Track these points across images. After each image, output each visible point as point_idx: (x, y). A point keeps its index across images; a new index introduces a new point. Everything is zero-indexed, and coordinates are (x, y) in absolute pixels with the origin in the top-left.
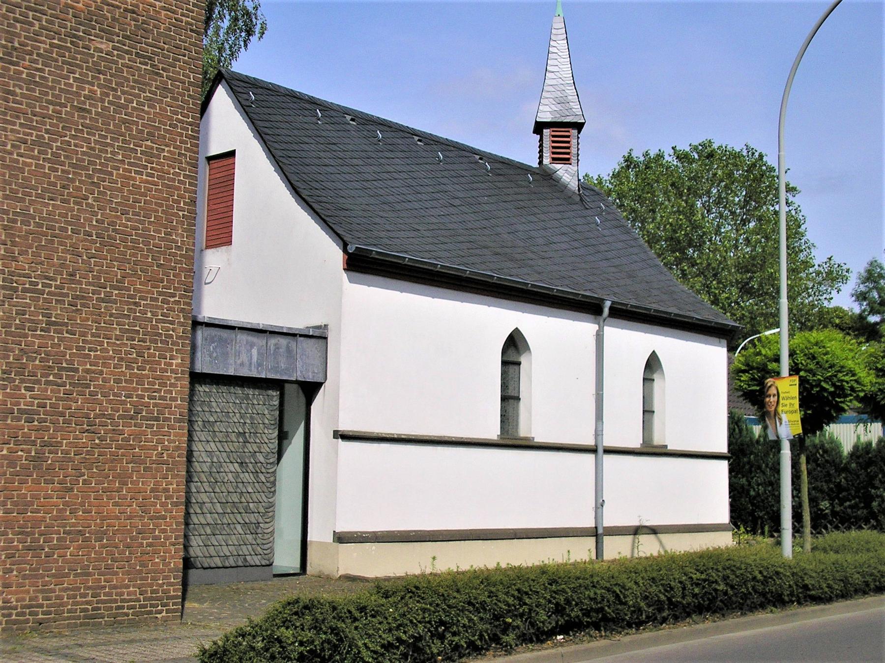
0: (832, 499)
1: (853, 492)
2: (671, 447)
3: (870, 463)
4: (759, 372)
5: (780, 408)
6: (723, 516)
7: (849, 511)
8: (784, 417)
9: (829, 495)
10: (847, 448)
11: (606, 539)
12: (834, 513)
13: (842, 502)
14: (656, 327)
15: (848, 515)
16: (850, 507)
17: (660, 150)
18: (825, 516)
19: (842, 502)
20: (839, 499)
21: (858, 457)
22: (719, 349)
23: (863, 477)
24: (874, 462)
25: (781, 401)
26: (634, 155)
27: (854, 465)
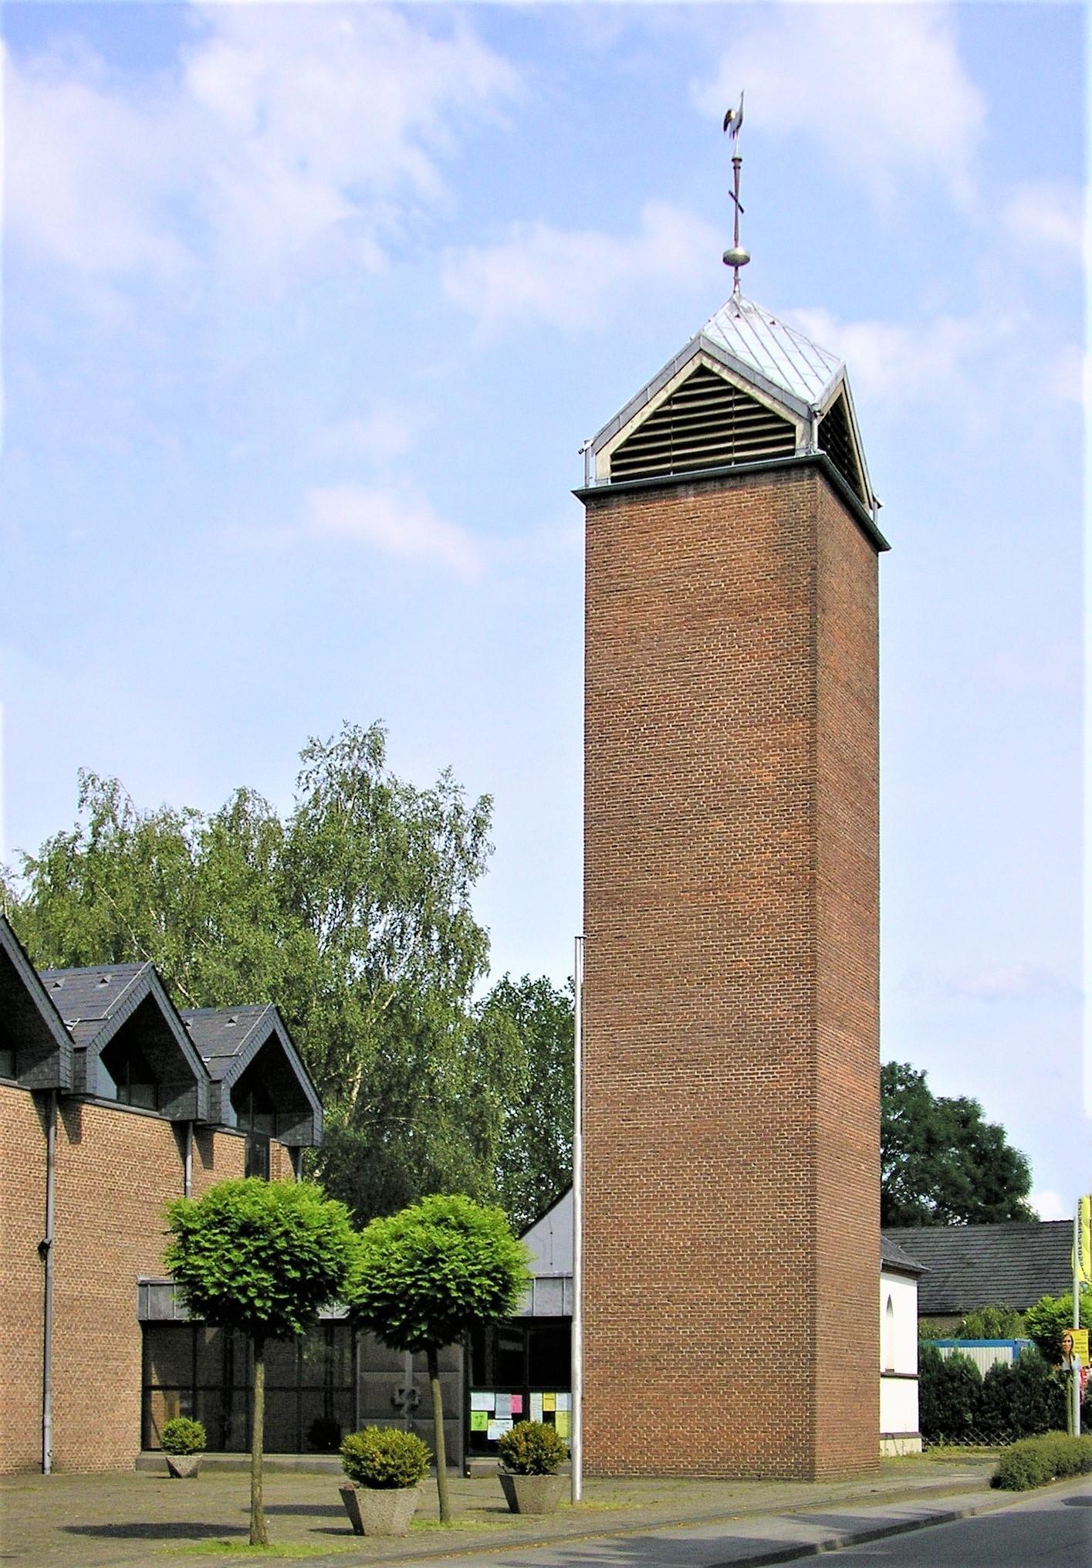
0: (973, 1412)
1: (993, 1405)
2: (897, 1371)
3: (1008, 1381)
4: (1050, 1324)
5: (1074, 1350)
6: (914, 1426)
7: (990, 1421)
8: (1076, 1355)
9: (970, 1408)
10: (984, 1367)
11: (266, 1477)
12: (976, 1424)
13: (983, 1415)
14: (891, 1275)
15: (989, 1424)
16: (991, 1418)
17: (544, 977)
18: (968, 1426)
19: (983, 1415)
20: (980, 1411)
21: (997, 1376)
22: (911, 1287)
23: (1003, 1393)
24: (1012, 1380)
25: (1075, 1345)
26: (511, 980)
27: (994, 1383)
